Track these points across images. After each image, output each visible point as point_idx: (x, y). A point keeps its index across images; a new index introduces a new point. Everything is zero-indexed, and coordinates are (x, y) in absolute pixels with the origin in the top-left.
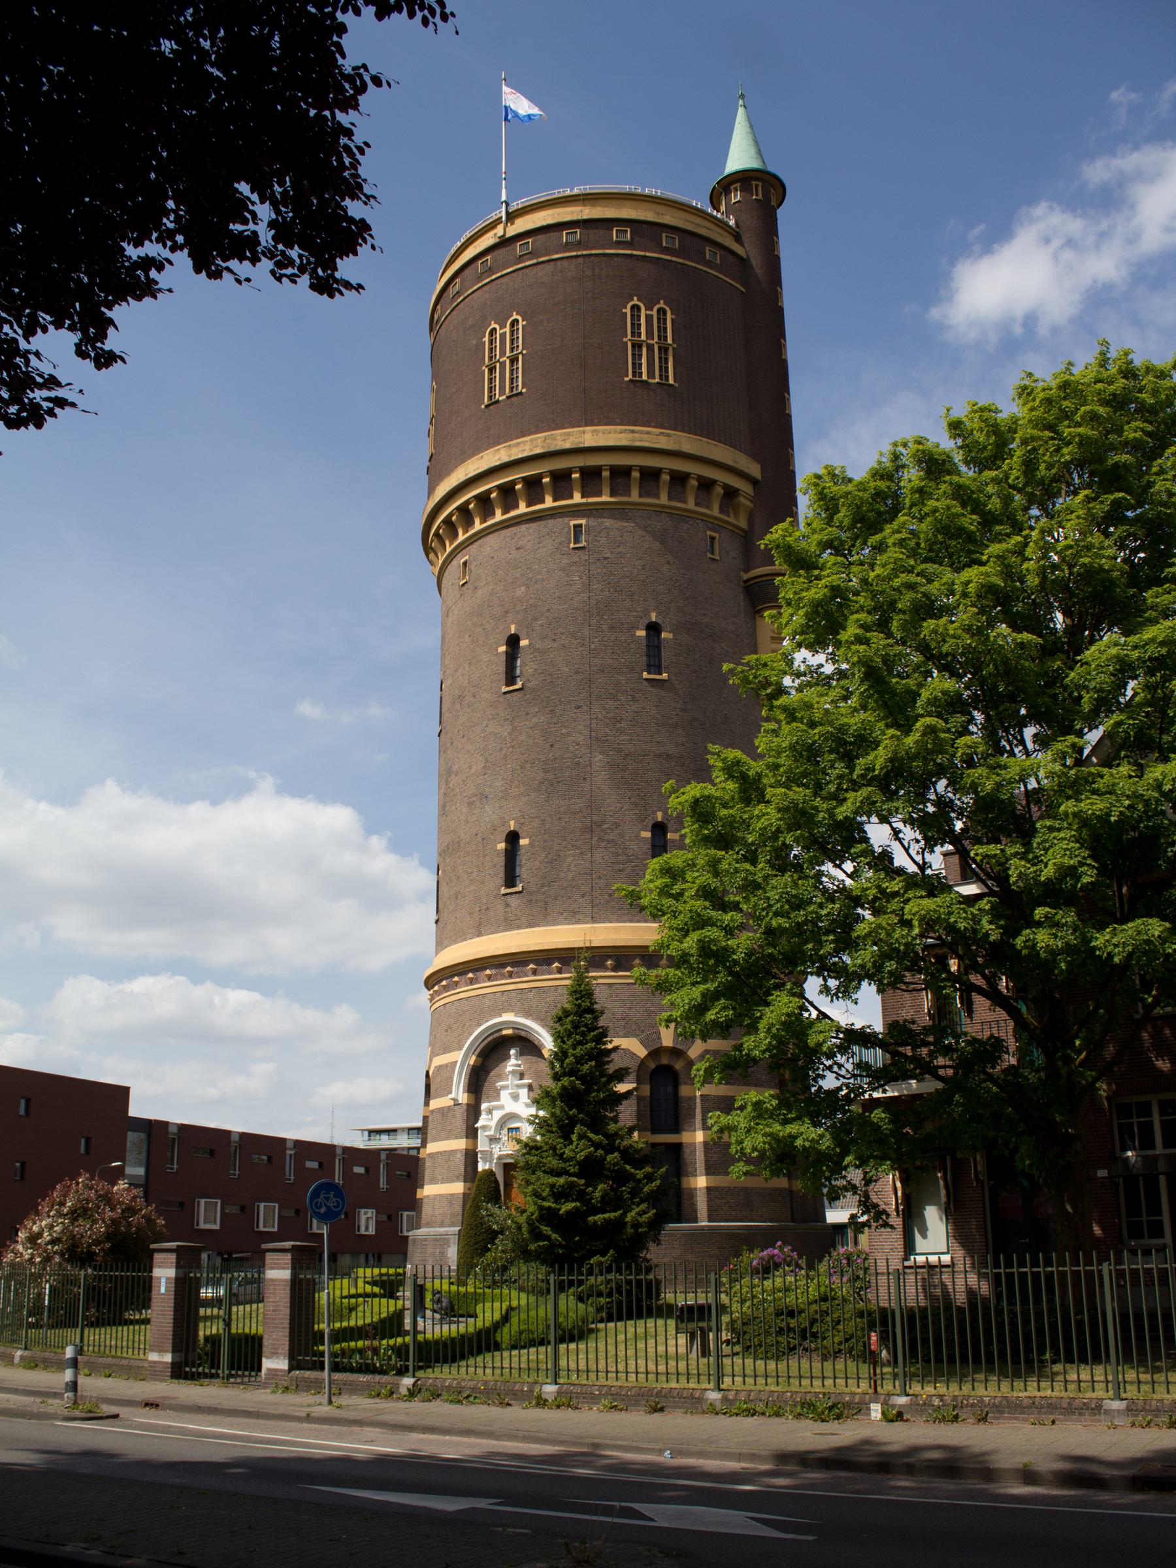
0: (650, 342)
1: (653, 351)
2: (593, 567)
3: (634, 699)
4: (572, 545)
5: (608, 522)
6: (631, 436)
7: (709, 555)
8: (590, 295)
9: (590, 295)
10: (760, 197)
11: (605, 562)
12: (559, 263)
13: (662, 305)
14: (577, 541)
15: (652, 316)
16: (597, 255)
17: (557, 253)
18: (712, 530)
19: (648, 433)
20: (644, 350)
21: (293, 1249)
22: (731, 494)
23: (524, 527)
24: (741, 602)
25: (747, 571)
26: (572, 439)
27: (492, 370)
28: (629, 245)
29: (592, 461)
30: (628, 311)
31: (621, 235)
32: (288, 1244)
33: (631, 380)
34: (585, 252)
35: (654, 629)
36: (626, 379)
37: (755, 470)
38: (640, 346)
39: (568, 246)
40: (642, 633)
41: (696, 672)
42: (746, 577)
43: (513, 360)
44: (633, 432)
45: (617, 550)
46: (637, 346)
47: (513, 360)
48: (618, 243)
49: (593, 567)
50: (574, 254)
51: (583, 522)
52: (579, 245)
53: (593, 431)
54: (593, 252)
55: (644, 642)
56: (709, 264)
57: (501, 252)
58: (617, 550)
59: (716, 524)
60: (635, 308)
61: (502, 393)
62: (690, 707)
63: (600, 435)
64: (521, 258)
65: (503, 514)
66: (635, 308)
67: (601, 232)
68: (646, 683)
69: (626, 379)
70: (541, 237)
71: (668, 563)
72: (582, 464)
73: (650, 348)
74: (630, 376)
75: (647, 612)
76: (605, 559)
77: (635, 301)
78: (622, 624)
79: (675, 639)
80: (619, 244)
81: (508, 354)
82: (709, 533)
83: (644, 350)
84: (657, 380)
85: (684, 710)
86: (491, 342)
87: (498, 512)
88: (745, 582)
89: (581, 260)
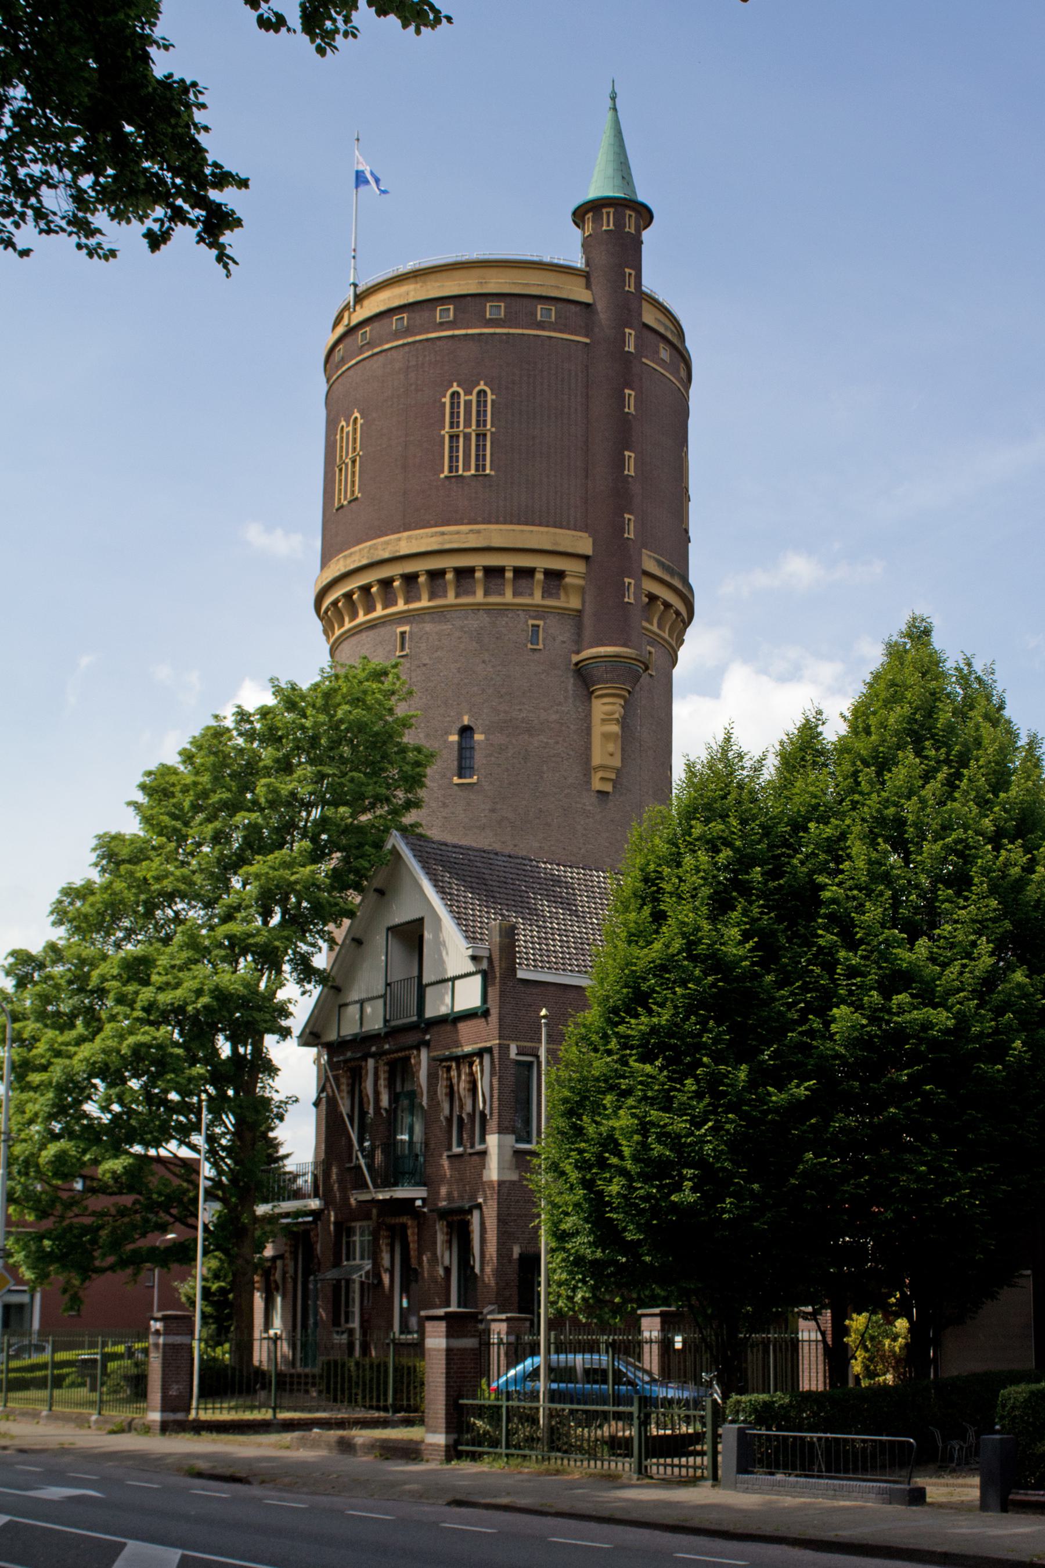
0: (467, 430)
1: (470, 440)
2: (413, 674)
3: (445, 805)
4: (398, 654)
5: (428, 627)
6: (440, 539)
7: (530, 646)
8: (413, 387)
9: (413, 387)
10: (612, 227)
11: (424, 669)
12: (389, 353)
13: (482, 386)
14: (402, 649)
15: (471, 401)
16: (420, 341)
17: (387, 343)
18: (535, 618)
19: (458, 533)
20: (461, 440)
21: (662, 1315)
22: (555, 576)
23: (364, 635)
24: (570, 687)
25: (578, 652)
26: (390, 548)
27: (341, 470)
28: (452, 325)
29: (409, 568)
30: (447, 400)
31: (445, 314)
32: (657, 1311)
33: (446, 477)
34: (410, 340)
35: (466, 731)
36: (442, 476)
37: (584, 545)
38: (458, 436)
39: (397, 335)
40: (454, 738)
41: (507, 770)
42: (575, 658)
43: (354, 462)
44: (443, 534)
45: (436, 655)
46: (454, 438)
47: (354, 462)
48: (441, 324)
49: (413, 674)
50: (400, 342)
51: (407, 628)
52: (408, 331)
53: (409, 538)
54: (418, 338)
55: (456, 747)
56: (541, 326)
57: (348, 340)
58: (436, 655)
59: (540, 612)
60: (455, 395)
61: (467, 468)
62: (499, 806)
63: (414, 541)
64: (361, 349)
65: (384, 609)
66: (455, 395)
67: (426, 314)
68: (456, 788)
69: (442, 476)
70: (376, 325)
71: (484, 662)
72: (401, 572)
73: (467, 437)
74: (446, 473)
75: (460, 716)
76: (425, 665)
77: (455, 388)
78: (437, 731)
79: (487, 739)
80: (442, 326)
81: (350, 456)
82: (531, 622)
83: (461, 440)
84: (473, 472)
85: (493, 811)
86: (342, 438)
87: (379, 607)
88: (577, 664)
89: (407, 349)
